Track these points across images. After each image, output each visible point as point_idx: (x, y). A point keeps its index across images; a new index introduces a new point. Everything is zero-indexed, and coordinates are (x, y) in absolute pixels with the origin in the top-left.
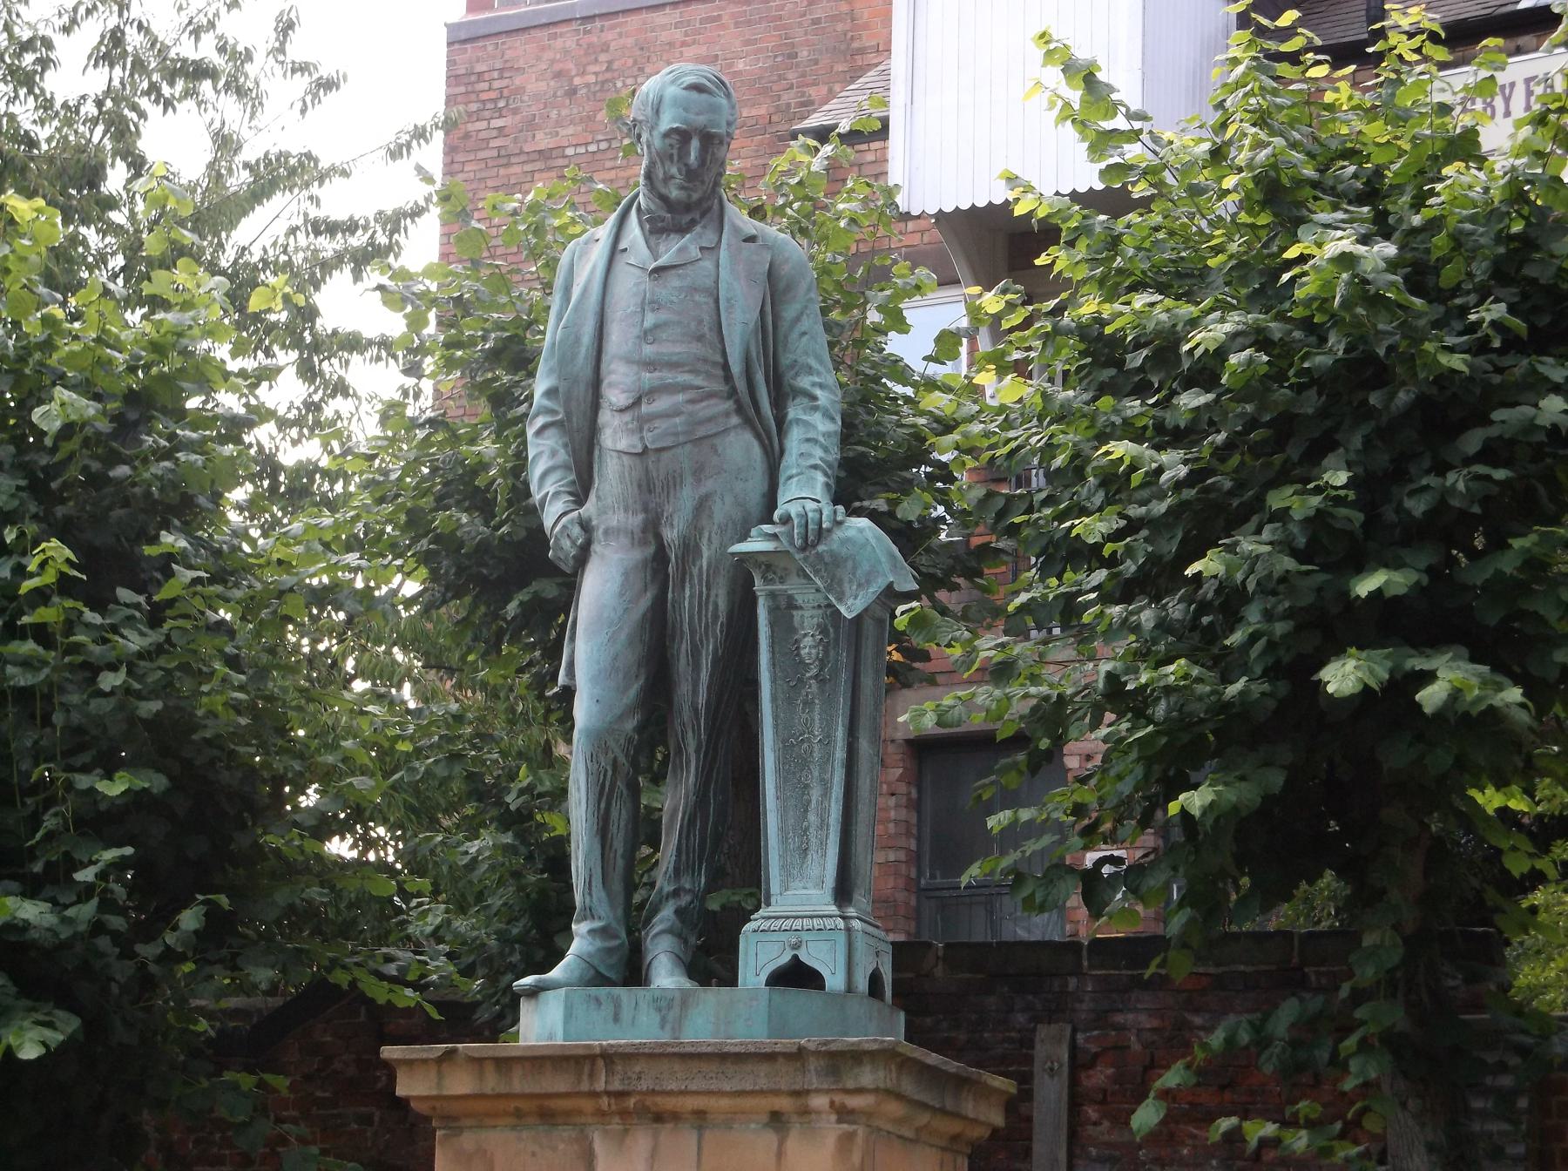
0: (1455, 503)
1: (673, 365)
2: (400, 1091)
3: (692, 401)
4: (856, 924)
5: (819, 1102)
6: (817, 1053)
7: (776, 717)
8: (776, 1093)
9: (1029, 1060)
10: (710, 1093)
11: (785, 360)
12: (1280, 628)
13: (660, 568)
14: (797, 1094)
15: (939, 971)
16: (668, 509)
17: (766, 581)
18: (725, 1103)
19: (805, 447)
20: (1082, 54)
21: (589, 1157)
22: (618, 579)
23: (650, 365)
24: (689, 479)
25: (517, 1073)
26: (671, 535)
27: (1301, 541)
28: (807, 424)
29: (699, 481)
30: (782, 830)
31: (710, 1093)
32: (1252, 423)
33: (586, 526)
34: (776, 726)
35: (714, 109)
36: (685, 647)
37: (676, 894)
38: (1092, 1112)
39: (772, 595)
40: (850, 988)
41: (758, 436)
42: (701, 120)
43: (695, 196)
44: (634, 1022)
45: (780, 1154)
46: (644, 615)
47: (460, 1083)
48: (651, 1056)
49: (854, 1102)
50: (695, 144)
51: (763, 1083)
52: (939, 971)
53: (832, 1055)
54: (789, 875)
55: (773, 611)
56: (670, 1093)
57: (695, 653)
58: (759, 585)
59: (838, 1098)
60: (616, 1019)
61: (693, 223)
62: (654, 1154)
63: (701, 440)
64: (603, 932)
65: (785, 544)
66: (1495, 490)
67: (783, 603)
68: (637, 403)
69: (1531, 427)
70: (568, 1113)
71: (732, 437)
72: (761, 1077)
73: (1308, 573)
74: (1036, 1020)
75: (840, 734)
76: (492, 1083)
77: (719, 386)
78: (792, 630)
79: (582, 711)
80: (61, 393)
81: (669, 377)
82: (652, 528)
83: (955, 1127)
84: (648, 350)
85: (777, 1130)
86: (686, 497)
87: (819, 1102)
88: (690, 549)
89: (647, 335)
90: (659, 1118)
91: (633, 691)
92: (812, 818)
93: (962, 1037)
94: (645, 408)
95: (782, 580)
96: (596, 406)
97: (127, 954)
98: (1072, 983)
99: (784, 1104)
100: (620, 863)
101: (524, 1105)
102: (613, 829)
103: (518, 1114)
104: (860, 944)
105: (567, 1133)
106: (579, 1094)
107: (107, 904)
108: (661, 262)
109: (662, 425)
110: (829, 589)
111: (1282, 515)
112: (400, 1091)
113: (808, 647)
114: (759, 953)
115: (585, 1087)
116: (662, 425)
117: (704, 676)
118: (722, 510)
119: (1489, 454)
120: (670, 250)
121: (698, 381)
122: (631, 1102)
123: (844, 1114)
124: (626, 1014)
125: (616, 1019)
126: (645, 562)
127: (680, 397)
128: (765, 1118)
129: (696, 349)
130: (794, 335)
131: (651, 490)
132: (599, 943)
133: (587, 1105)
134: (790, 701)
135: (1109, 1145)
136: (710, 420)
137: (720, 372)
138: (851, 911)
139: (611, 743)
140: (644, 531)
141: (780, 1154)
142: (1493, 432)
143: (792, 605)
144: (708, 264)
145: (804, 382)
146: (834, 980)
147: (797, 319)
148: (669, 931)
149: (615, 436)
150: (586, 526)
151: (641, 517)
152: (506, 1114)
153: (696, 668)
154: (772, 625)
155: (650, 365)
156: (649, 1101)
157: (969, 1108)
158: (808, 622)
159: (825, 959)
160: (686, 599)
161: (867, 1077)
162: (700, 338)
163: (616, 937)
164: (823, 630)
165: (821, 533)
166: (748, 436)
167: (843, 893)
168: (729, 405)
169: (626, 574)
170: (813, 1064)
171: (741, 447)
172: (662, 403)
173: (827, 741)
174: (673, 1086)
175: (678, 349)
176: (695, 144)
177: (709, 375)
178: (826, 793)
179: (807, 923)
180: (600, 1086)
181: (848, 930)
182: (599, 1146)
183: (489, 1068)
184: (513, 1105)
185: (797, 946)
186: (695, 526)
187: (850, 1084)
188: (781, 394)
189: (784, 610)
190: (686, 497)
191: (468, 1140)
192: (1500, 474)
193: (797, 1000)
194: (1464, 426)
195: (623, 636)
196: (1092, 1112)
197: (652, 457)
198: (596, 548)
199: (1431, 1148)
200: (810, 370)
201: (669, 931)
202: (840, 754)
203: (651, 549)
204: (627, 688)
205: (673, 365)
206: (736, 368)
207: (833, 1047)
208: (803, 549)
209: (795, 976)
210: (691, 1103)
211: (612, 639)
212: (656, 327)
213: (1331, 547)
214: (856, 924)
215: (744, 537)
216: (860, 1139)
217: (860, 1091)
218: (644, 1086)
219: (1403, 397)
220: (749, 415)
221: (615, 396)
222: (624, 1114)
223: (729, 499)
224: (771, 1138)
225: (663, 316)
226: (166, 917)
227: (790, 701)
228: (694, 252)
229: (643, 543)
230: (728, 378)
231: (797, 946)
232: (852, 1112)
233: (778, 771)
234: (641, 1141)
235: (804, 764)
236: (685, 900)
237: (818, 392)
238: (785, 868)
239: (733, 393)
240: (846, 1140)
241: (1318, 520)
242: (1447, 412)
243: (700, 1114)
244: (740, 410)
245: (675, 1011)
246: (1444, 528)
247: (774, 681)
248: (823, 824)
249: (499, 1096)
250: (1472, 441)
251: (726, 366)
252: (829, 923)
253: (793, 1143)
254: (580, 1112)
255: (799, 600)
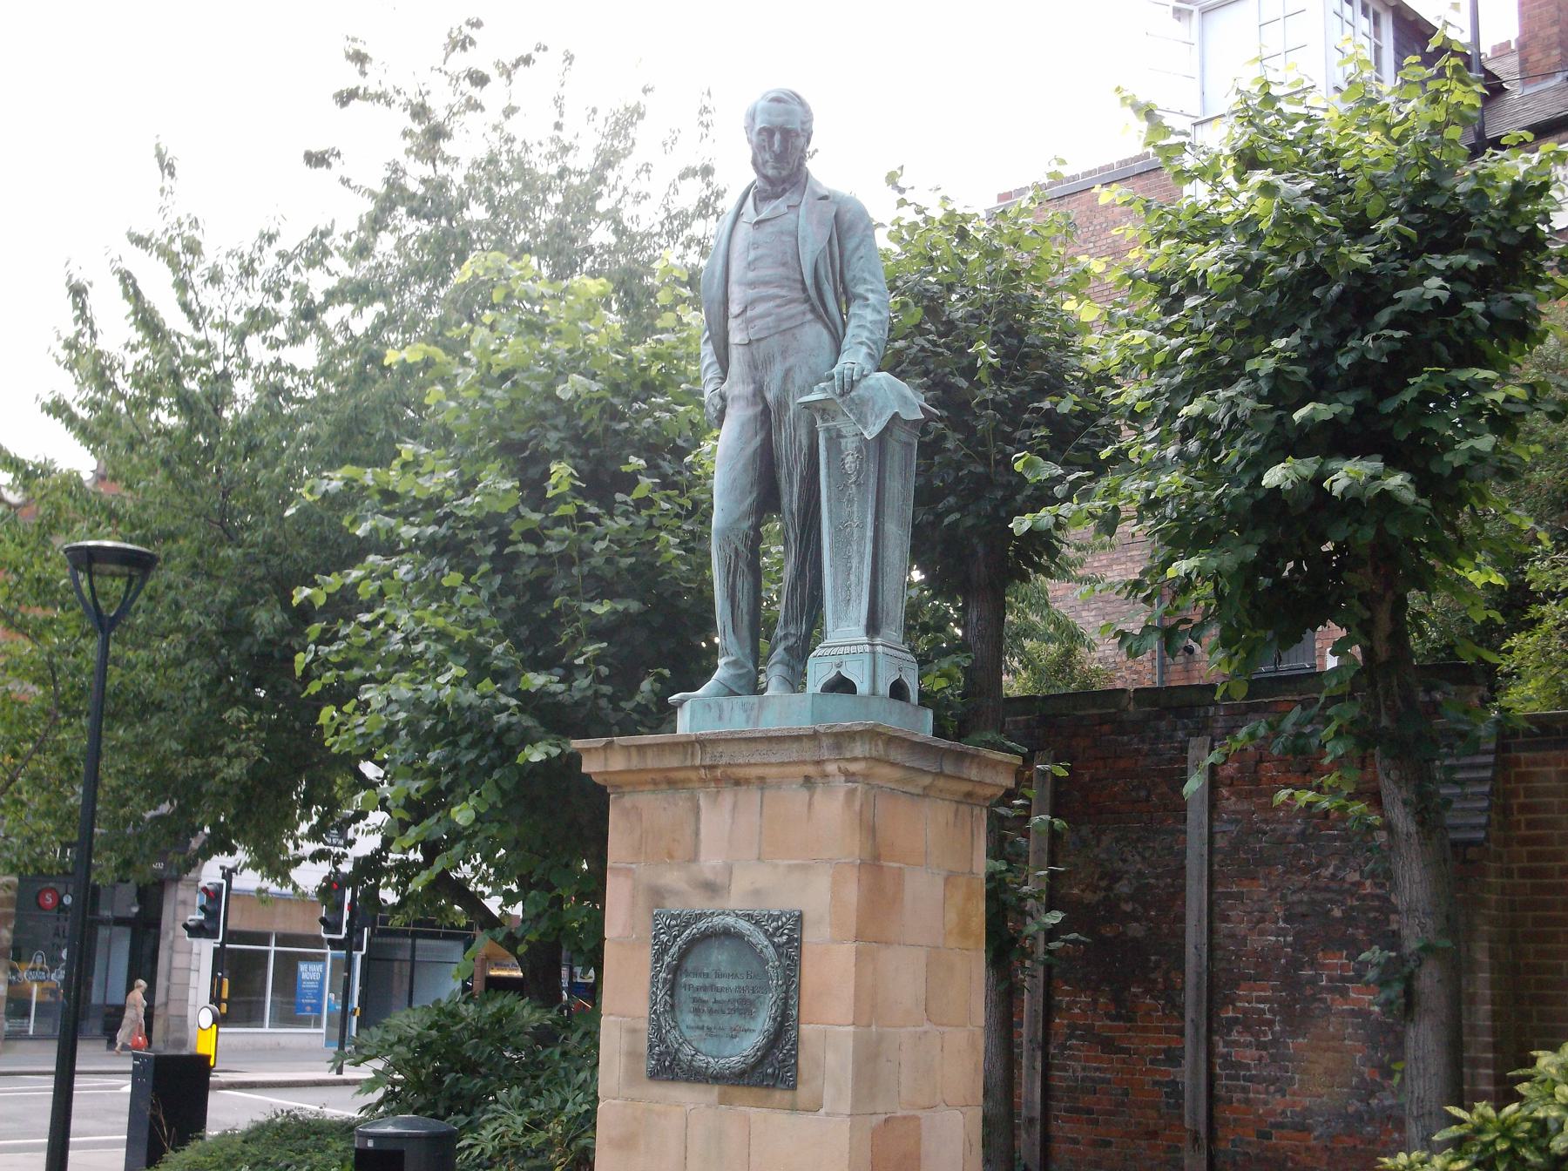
0: (1371, 357)
1: (766, 283)
2: (584, 770)
3: (778, 306)
4: (879, 649)
5: (831, 768)
6: (825, 734)
7: (830, 511)
8: (804, 762)
9: (1185, 760)
10: (765, 764)
11: (848, 276)
12: (1253, 449)
13: (767, 418)
14: (818, 763)
15: (1131, 707)
16: (767, 379)
17: (825, 421)
18: (774, 771)
19: (857, 331)
20: (1142, 99)
21: (697, 811)
22: (738, 429)
23: (752, 284)
24: (779, 358)
25: (650, 754)
26: (770, 396)
27: (1265, 391)
28: (861, 316)
29: (785, 358)
30: (834, 587)
31: (765, 764)
32: (1237, 316)
33: (723, 398)
34: (830, 518)
35: (789, 113)
36: (783, 472)
37: (786, 637)
38: (1225, 792)
39: (828, 430)
40: (874, 693)
41: (826, 326)
42: (779, 120)
43: (784, 173)
44: (736, 718)
45: (810, 805)
46: (755, 452)
47: (617, 763)
48: (726, 740)
49: (854, 767)
50: (777, 137)
51: (795, 757)
52: (1131, 707)
53: (837, 735)
54: (839, 618)
55: (829, 440)
56: (739, 765)
57: (790, 475)
58: (819, 423)
59: (843, 765)
60: (720, 718)
61: (784, 191)
62: (735, 806)
63: (786, 331)
64: (735, 664)
65: (829, 395)
66: (1399, 346)
67: (834, 434)
68: (744, 311)
69: (1422, 300)
70: (683, 781)
71: (807, 328)
72: (793, 752)
73: (1265, 411)
74: (1190, 735)
75: (870, 519)
76: (635, 763)
77: (799, 295)
78: (840, 452)
79: (716, 520)
80: (575, 377)
81: (764, 291)
82: (759, 393)
83: (966, 787)
84: (751, 275)
85: (809, 789)
86: (777, 370)
87: (831, 768)
88: (782, 404)
89: (750, 265)
90: (737, 783)
91: (749, 500)
92: (852, 577)
93: (1146, 747)
94: (749, 313)
95: (833, 419)
96: (726, 318)
97: (617, 708)
98: (1212, 709)
99: (810, 770)
100: (746, 618)
101: (657, 776)
102: (739, 595)
103: (655, 783)
104: (881, 661)
105: (684, 794)
106: (686, 768)
107: (599, 679)
108: (762, 216)
109: (759, 323)
110: (859, 421)
111: (1254, 376)
112: (584, 770)
113: (850, 462)
114: (819, 671)
115: (688, 763)
116: (759, 323)
117: (796, 489)
118: (799, 378)
119: (1394, 324)
120: (767, 211)
121: (783, 292)
122: (719, 772)
123: (849, 776)
124: (726, 715)
125: (720, 718)
126: (755, 417)
127: (771, 304)
128: (801, 780)
129: (781, 271)
130: (854, 260)
131: (756, 367)
132: (732, 671)
133: (693, 775)
134: (839, 500)
135: (1234, 812)
136: (791, 317)
137: (799, 286)
138: (878, 640)
139: (732, 537)
140: (754, 395)
141: (810, 805)
142: (1398, 307)
143: (840, 436)
144: (792, 216)
145: (860, 289)
146: (863, 687)
147: (857, 248)
148: (781, 662)
149: (736, 337)
150: (723, 398)
151: (752, 387)
152: (646, 783)
153: (791, 486)
154: (828, 450)
155: (752, 284)
156: (729, 771)
157: (973, 773)
158: (849, 444)
159: (858, 674)
160: (782, 440)
161: (859, 749)
162: (784, 264)
163: (743, 667)
164: (859, 451)
165: (853, 384)
166: (819, 327)
167: (873, 627)
168: (806, 307)
169: (743, 425)
170: (826, 742)
171: (814, 334)
172: (760, 309)
173: (862, 526)
174: (741, 761)
175: (770, 272)
176: (777, 137)
177: (791, 289)
178: (861, 561)
179: (847, 649)
180: (698, 762)
181: (874, 653)
182: (702, 802)
183: (634, 752)
184: (651, 776)
185: (839, 666)
186: (784, 389)
187: (848, 756)
188: (847, 296)
189: (835, 438)
190: (777, 370)
191: (627, 801)
192: (1398, 334)
193: (839, 700)
194: (1379, 308)
195: (739, 466)
196: (1225, 792)
197: (755, 346)
198: (728, 410)
199: (1405, 803)
200: (865, 281)
201: (781, 662)
202: (870, 533)
203: (760, 407)
204: (741, 502)
205: (766, 283)
206: (809, 281)
207: (834, 730)
208: (842, 395)
209: (841, 685)
210: (754, 772)
211: (732, 468)
212: (756, 259)
213: (1282, 393)
214: (879, 649)
215: (811, 391)
216: (859, 793)
217: (855, 759)
218: (723, 761)
219: (1336, 289)
220: (819, 311)
221: (734, 309)
222: (717, 780)
223: (805, 370)
224: (804, 794)
225: (760, 252)
226: (634, 688)
227: (839, 500)
228: (784, 209)
229: (755, 404)
230: (805, 289)
231: (839, 666)
232: (853, 774)
233: (831, 548)
234: (727, 797)
235: (849, 543)
236: (792, 641)
237: (870, 296)
238: (835, 612)
239: (808, 300)
240: (851, 793)
241: (1277, 374)
242: (1366, 296)
243: (762, 779)
244: (813, 310)
245: (755, 713)
246: (1362, 373)
247: (829, 487)
248: (860, 582)
249: (641, 771)
250: (1384, 316)
251: (803, 282)
252: (860, 648)
253: (818, 796)
254: (690, 780)
255: (844, 432)
